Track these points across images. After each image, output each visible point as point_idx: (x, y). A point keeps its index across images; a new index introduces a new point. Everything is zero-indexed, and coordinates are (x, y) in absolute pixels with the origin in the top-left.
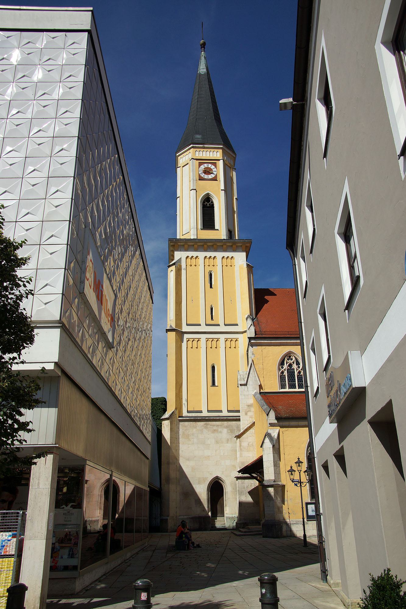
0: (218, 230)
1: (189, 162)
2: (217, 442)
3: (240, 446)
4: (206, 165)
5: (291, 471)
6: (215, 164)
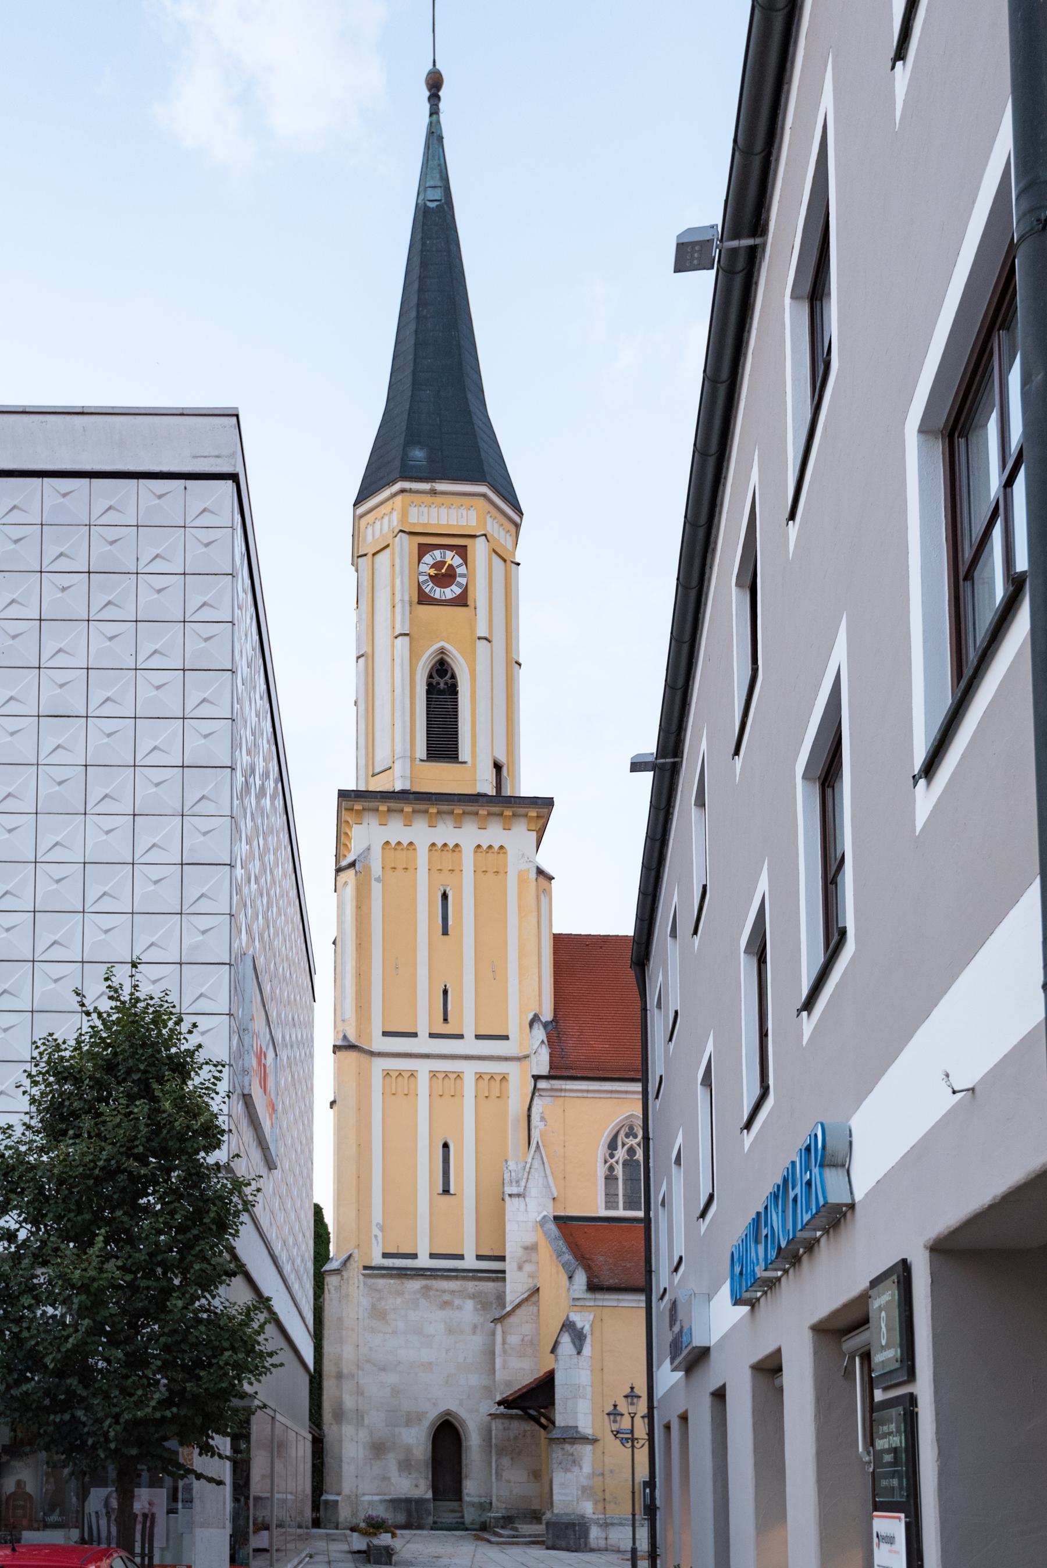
0: (465, 763)
1: (390, 541)
2: (450, 1331)
3: (504, 1343)
4: (437, 553)
5: (615, 1414)
6: (462, 552)
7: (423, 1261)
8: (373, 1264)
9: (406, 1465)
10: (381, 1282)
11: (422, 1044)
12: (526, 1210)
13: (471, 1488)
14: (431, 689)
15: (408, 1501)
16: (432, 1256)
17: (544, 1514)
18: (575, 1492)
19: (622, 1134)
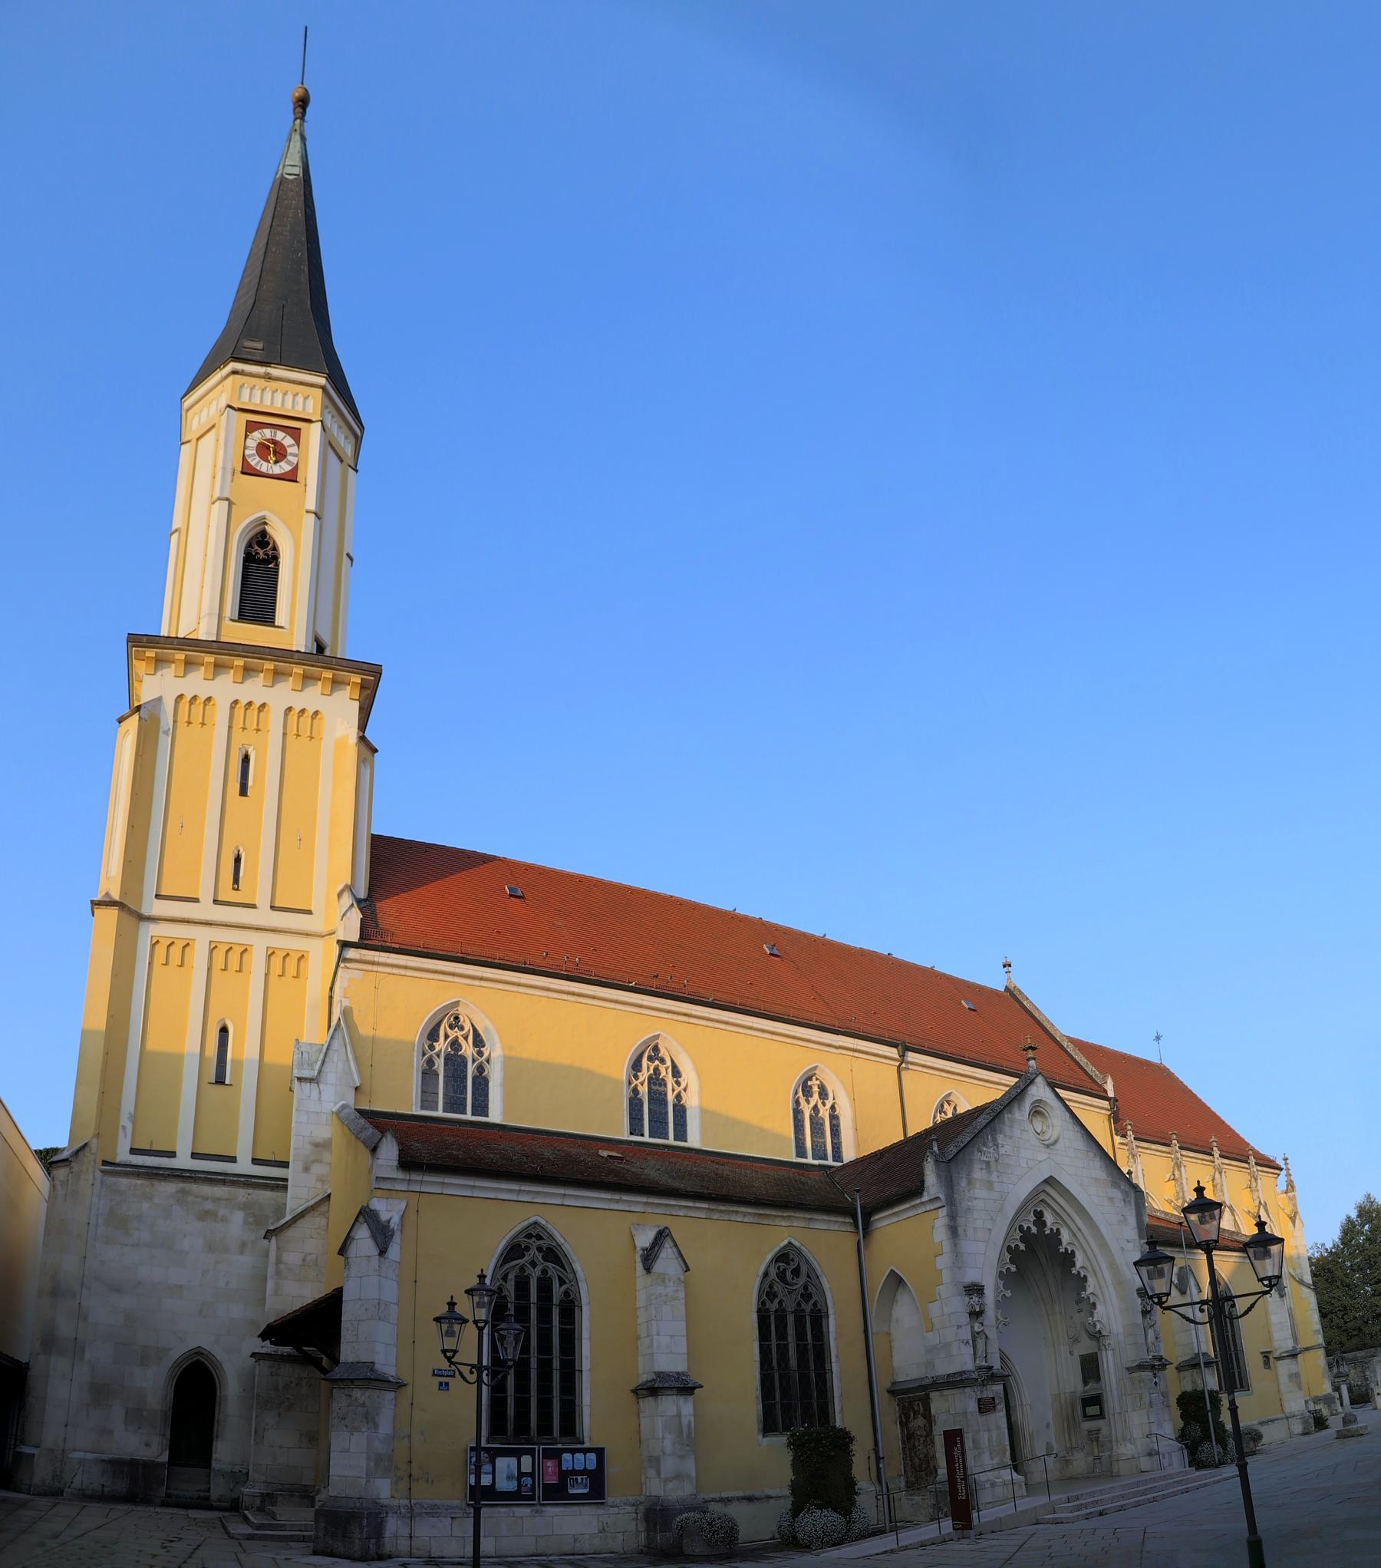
2: (210, 1248)
3: (279, 1261)
4: (268, 433)
6: (295, 433)
7: (183, 1161)
8: (117, 1161)
9: (135, 1416)
10: (124, 1182)
11: (205, 910)
12: (319, 1099)
13: (224, 1452)
14: (249, 559)
15: (133, 1464)
16: (195, 1155)
17: (318, 1492)
18: (364, 1463)
19: (444, 1025)
